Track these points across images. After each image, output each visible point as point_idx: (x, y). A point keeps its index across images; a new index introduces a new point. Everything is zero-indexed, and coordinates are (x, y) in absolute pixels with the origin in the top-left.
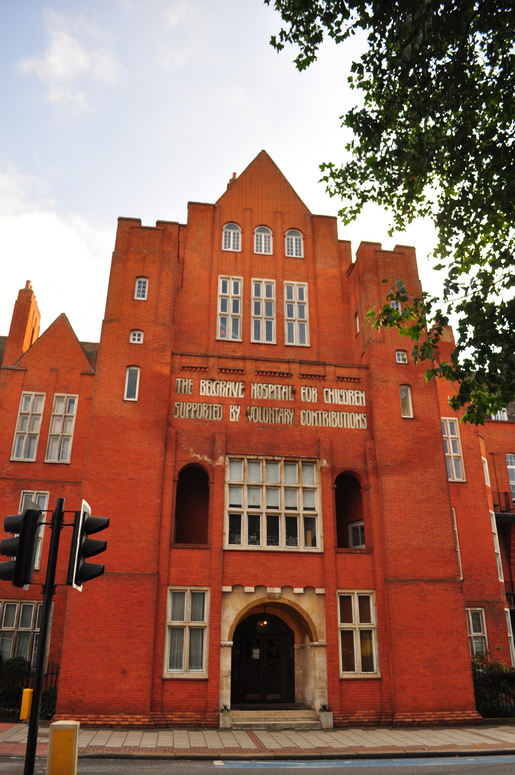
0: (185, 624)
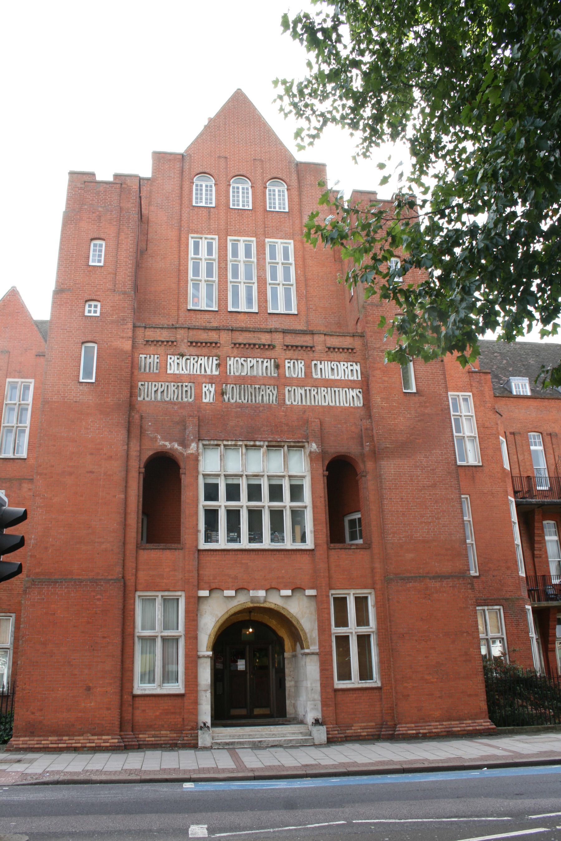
0: (157, 634)
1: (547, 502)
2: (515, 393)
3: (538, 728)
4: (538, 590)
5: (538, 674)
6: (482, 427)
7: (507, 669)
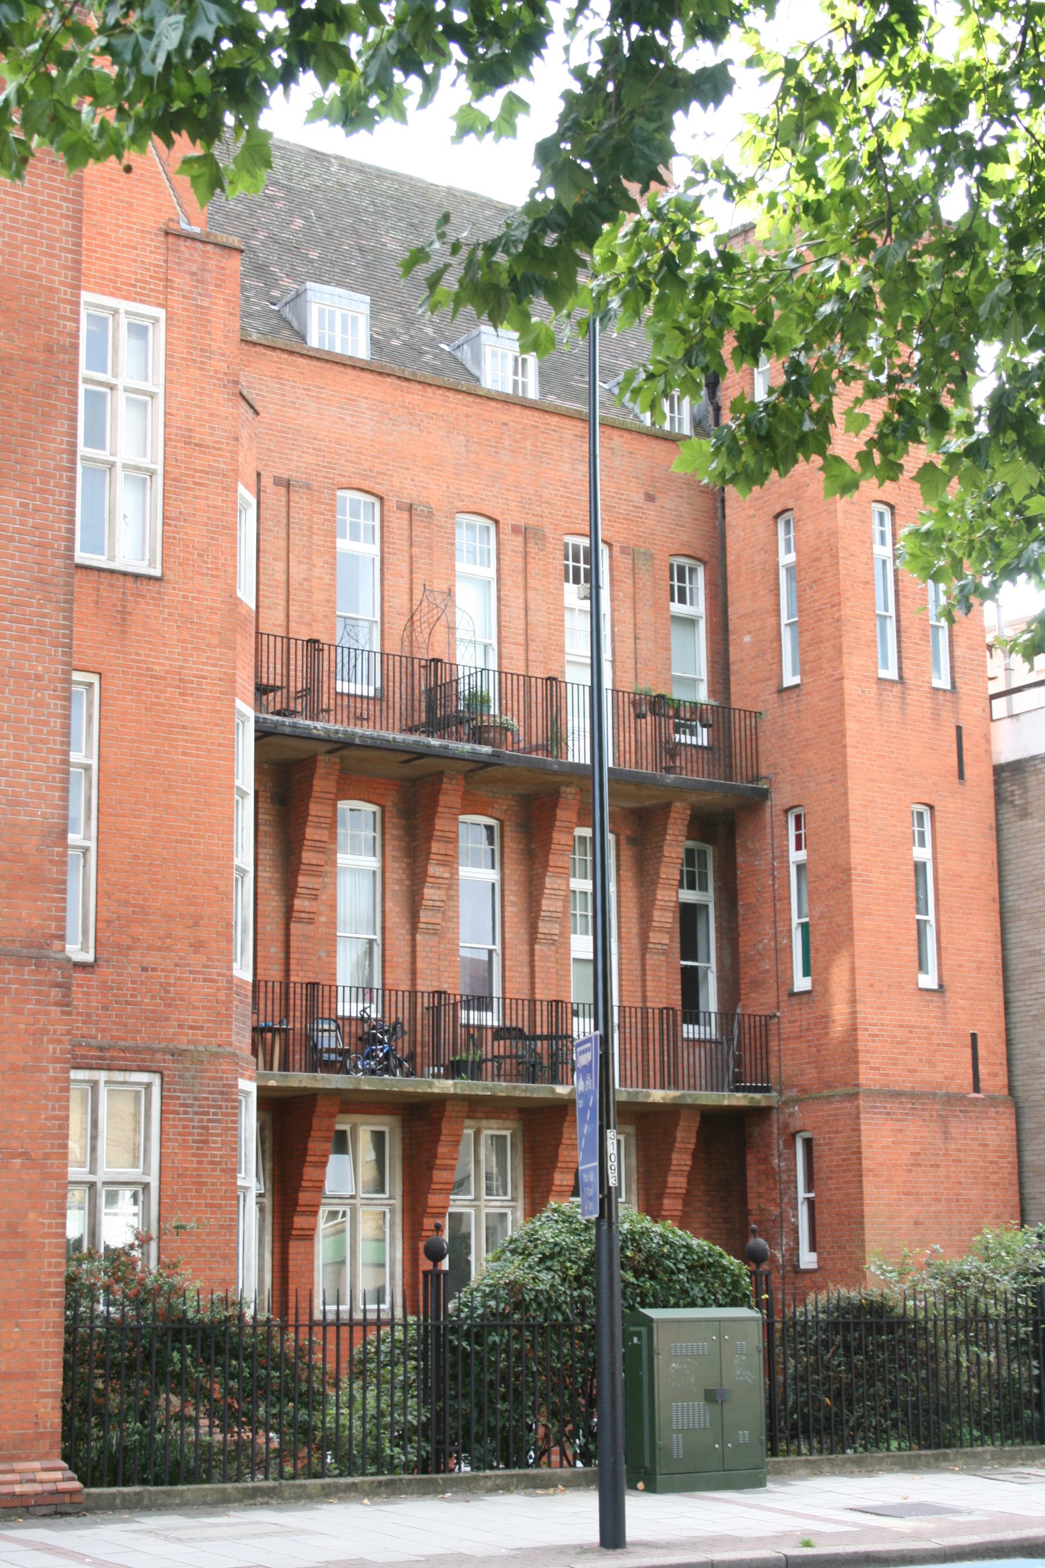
1: (362, 736)
2: (313, 341)
3: (223, 1491)
4: (286, 1031)
5: (249, 1313)
6: (181, 441)
7: (148, 1292)
